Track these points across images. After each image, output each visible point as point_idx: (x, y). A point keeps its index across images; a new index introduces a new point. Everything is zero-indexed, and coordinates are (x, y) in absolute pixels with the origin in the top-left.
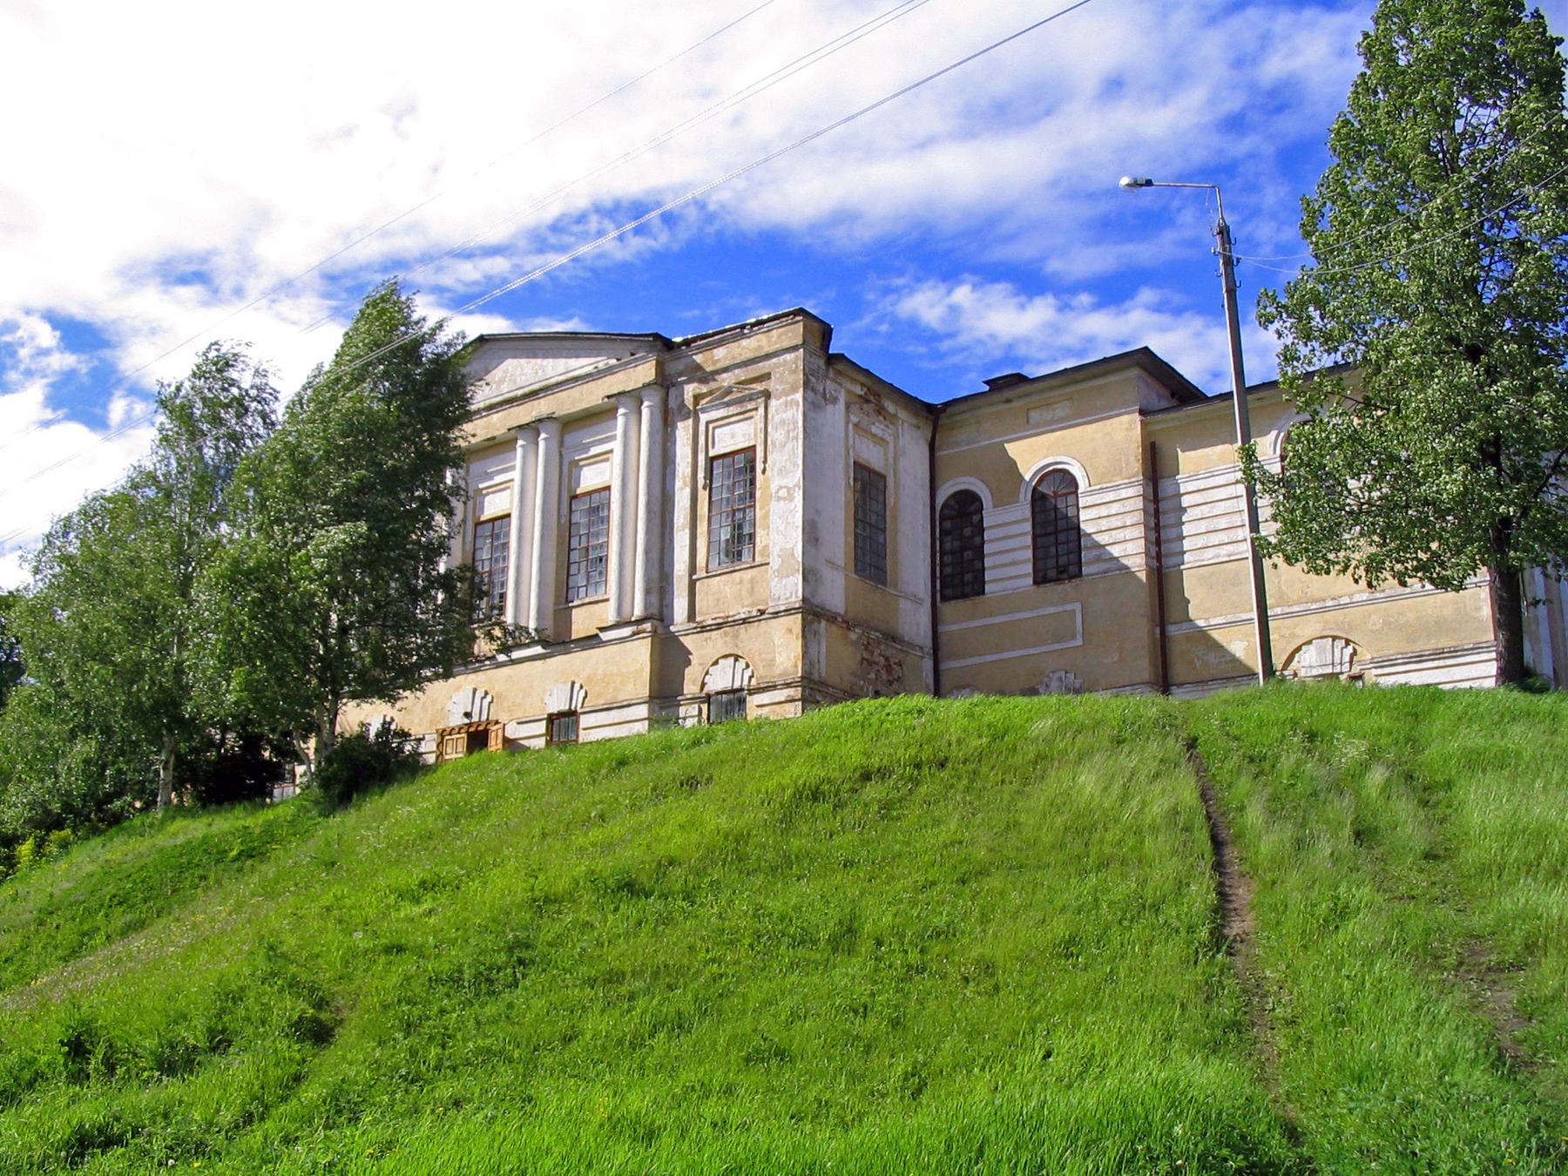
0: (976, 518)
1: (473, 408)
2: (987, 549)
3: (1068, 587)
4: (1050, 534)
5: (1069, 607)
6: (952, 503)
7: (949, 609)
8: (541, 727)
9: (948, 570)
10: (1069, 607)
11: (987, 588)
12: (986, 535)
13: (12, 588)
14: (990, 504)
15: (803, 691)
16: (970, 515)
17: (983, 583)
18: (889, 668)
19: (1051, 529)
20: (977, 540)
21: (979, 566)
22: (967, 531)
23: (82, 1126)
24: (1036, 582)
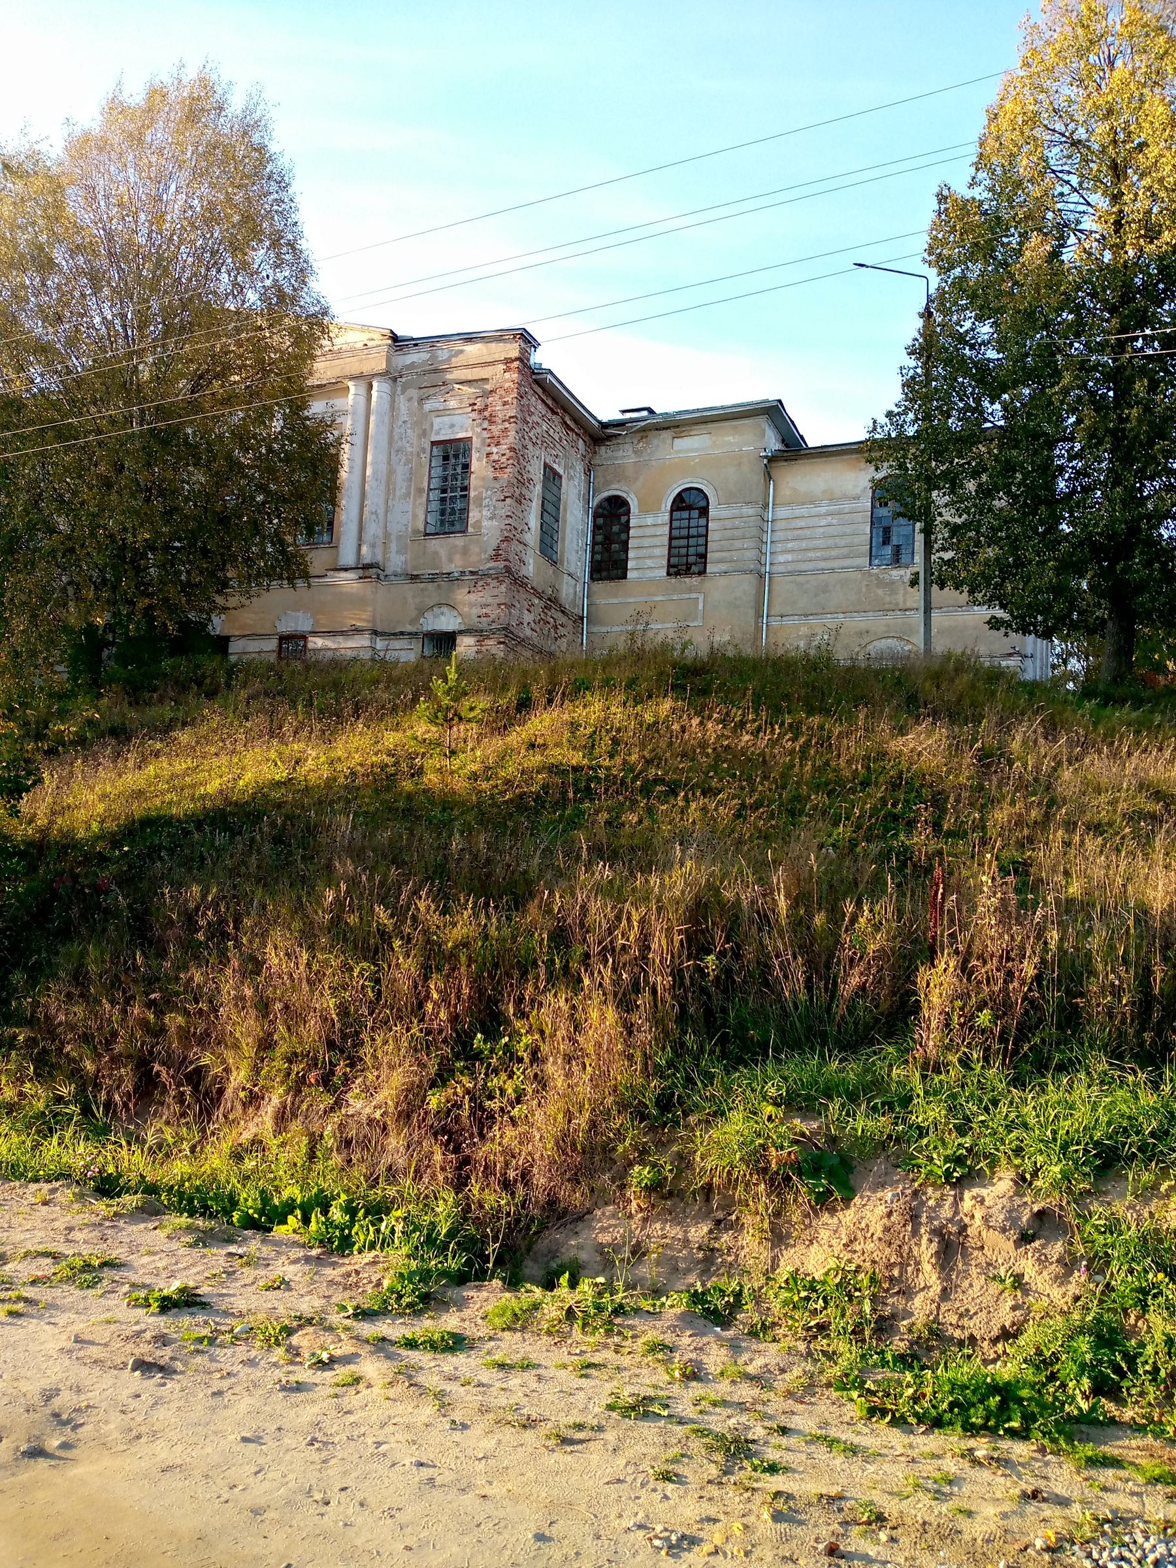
0: (624, 519)
1: (310, 382)
2: (631, 543)
3: (695, 581)
4: (693, 537)
5: (694, 595)
6: (606, 504)
7: (599, 586)
8: (273, 644)
9: (598, 557)
10: (694, 595)
11: (630, 575)
12: (632, 532)
13: (273, 148)
14: (637, 511)
15: (305, 646)
16: (619, 516)
17: (626, 569)
18: (556, 627)
19: (684, 532)
20: (623, 536)
21: (623, 557)
22: (615, 529)
23: (117, 755)
24: (669, 574)
